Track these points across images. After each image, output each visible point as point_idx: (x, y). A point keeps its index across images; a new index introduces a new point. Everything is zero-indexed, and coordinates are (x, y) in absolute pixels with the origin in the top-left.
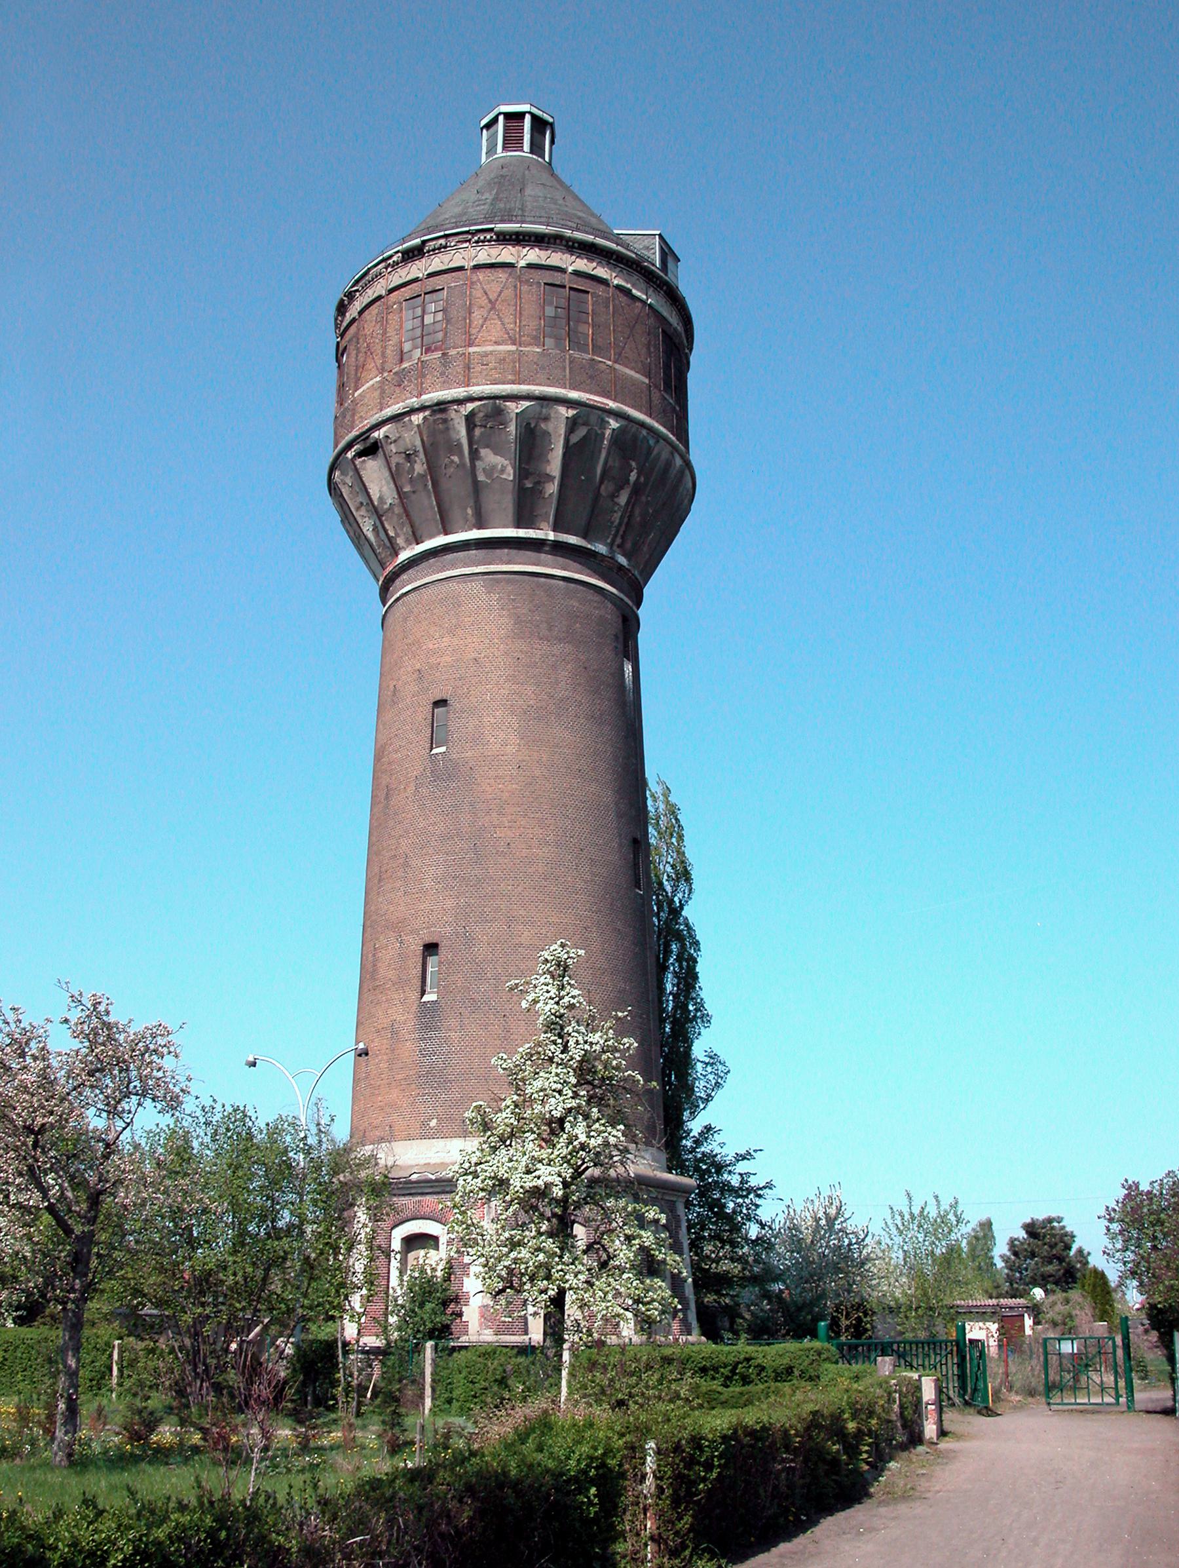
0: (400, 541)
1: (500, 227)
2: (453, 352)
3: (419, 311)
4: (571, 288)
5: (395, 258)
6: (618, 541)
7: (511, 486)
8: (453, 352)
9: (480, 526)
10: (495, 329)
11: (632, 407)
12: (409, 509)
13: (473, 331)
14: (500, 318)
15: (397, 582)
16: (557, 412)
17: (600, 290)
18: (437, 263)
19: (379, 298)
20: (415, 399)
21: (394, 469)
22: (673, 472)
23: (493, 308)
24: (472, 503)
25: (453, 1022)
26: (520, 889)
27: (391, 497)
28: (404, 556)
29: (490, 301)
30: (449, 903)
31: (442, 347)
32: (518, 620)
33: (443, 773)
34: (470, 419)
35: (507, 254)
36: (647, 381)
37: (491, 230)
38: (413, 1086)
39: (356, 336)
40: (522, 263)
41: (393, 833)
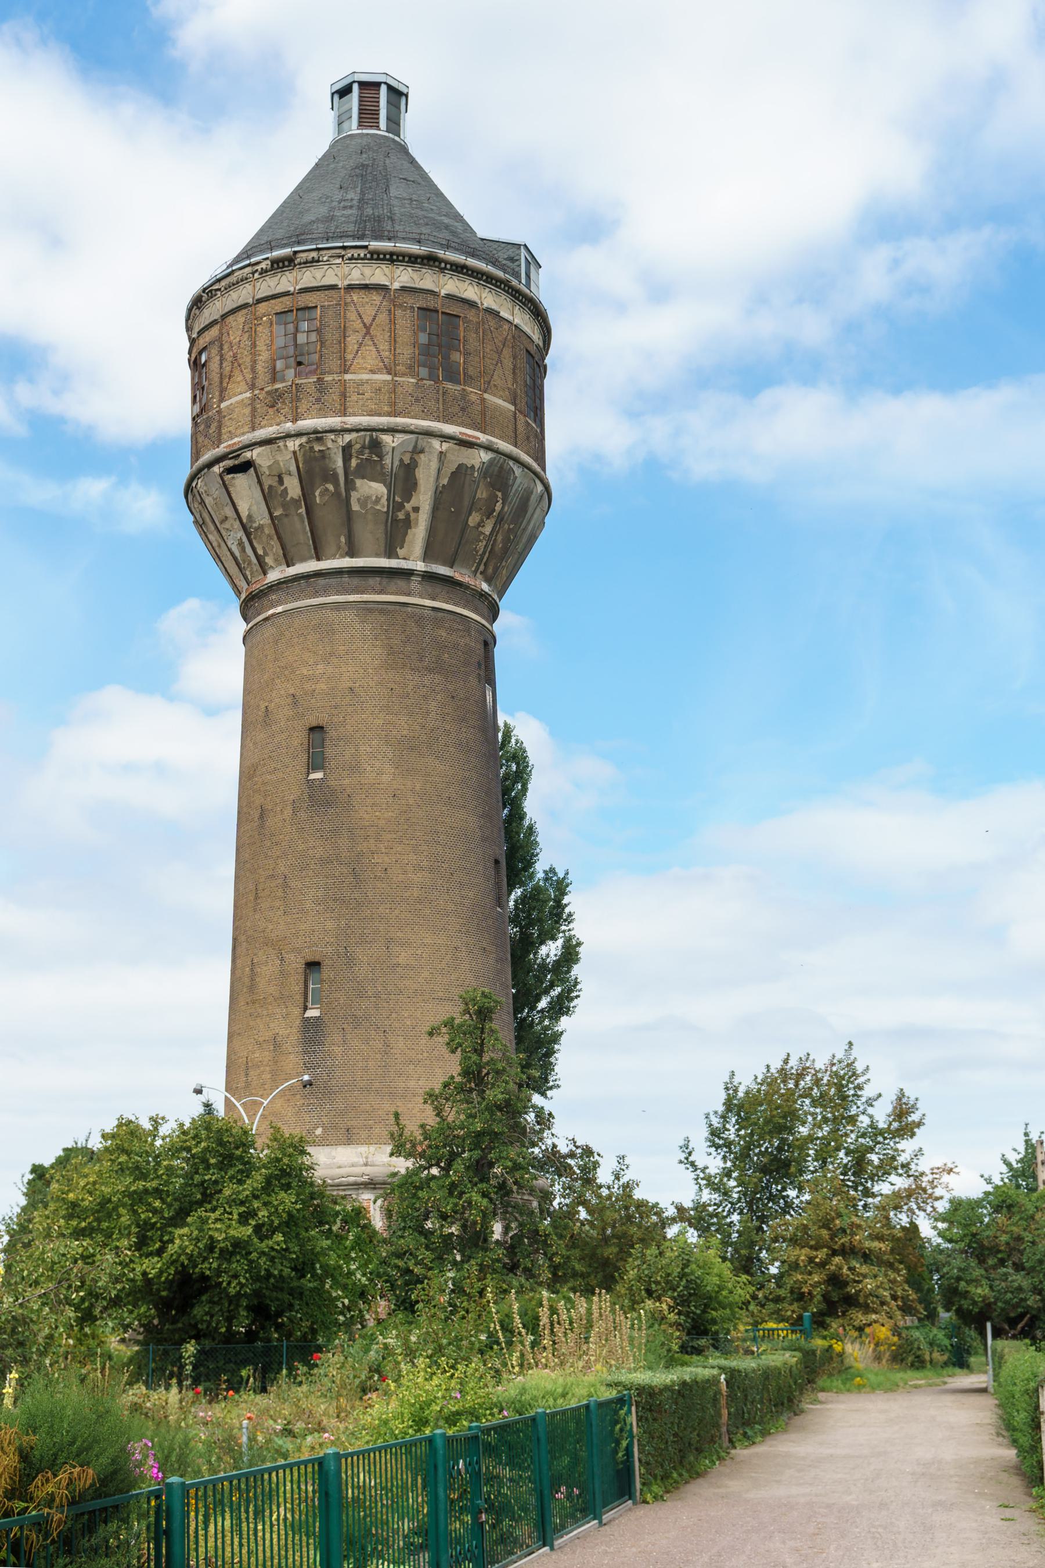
0: (269, 560)
1: (375, 245)
2: (328, 378)
3: (291, 327)
4: (443, 313)
5: (263, 265)
6: (482, 568)
7: (383, 517)
8: (328, 378)
9: (352, 553)
10: (369, 357)
11: (501, 438)
12: (281, 531)
13: (349, 357)
14: (375, 344)
15: (265, 601)
16: (431, 447)
17: (471, 315)
18: (309, 277)
19: (245, 306)
20: (289, 424)
21: (266, 491)
22: (533, 498)
23: (368, 333)
24: (346, 531)
25: (337, 1037)
26: (397, 912)
27: (262, 518)
28: (273, 576)
29: (365, 325)
30: (330, 925)
31: (319, 369)
32: (391, 651)
33: (320, 799)
34: (347, 450)
35: (378, 274)
36: (512, 408)
37: (366, 247)
38: (298, 1097)
39: (219, 341)
40: (396, 285)
41: (270, 854)
